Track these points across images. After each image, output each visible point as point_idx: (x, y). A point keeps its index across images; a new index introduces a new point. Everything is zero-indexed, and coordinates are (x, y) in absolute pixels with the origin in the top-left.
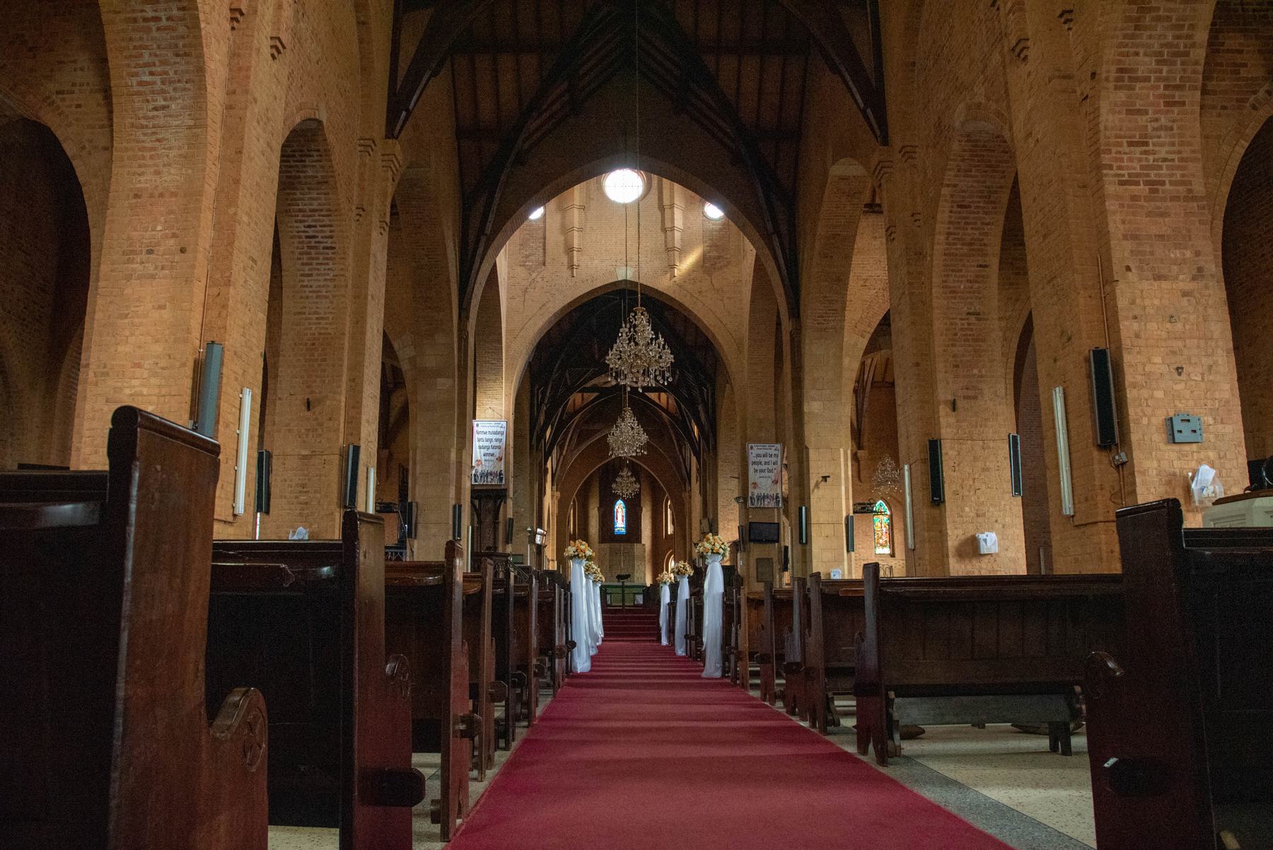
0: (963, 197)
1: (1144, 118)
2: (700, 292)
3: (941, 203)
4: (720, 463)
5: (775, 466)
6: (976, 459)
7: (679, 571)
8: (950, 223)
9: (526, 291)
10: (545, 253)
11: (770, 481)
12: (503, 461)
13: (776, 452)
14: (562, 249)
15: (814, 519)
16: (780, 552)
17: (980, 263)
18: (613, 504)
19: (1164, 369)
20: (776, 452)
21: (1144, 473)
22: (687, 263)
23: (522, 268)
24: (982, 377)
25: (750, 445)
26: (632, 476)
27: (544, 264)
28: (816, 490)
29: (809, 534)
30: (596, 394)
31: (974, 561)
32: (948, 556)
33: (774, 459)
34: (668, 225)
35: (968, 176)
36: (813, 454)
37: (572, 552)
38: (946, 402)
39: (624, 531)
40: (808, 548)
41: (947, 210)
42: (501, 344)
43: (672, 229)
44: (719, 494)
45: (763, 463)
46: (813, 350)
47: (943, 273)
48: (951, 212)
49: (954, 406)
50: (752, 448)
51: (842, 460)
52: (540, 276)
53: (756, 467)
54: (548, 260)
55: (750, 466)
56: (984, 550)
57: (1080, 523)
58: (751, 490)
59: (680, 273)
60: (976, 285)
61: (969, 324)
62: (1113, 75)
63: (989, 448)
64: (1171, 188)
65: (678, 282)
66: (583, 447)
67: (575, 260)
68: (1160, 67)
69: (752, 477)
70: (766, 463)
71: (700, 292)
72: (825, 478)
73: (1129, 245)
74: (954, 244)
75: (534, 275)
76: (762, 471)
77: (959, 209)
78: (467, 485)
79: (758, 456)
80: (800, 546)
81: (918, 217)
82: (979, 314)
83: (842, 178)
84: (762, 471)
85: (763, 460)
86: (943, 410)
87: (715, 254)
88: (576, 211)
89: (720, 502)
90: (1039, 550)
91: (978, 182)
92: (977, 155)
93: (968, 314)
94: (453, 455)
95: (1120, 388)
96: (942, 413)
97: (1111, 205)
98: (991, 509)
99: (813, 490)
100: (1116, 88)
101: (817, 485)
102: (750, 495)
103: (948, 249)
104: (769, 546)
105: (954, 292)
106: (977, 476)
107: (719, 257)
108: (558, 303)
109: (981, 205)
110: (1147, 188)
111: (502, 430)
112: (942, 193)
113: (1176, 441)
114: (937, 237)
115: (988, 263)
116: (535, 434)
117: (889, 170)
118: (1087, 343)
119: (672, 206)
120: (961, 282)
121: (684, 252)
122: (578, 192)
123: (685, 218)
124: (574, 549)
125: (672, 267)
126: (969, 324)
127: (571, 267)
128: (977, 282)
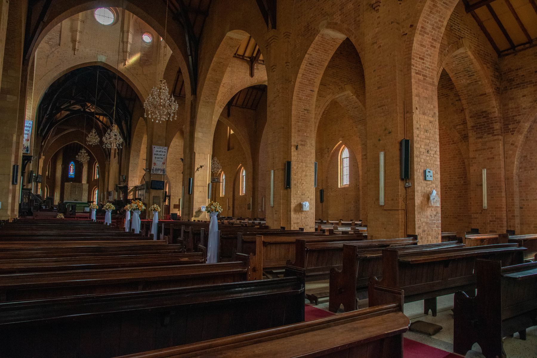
0: (312, 60)
1: (425, 49)
2: (137, 74)
3: (303, 61)
4: (132, 152)
5: (164, 157)
6: (303, 171)
7: (155, 209)
8: (305, 70)
9: (48, 56)
10: (60, 39)
11: (161, 163)
12: (29, 141)
13: (165, 151)
14: (70, 39)
15: (195, 184)
16: (163, 194)
17: (311, 89)
18: (69, 163)
19: (424, 150)
20: (165, 151)
21: (418, 191)
22: (132, 60)
23: (47, 44)
24: (307, 137)
25: (154, 146)
26: (86, 153)
27: (59, 45)
28: (197, 171)
29: (193, 190)
30: (68, 113)
31: (300, 213)
32: (290, 211)
33: (164, 153)
34: (125, 40)
35: (316, 52)
36: (197, 156)
37: (135, 207)
38: (294, 145)
39: (73, 176)
40: (192, 196)
41: (305, 64)
42: (33, 81)
43: (127, 42)
44: (130, 165)
45: (159, 155)
46: (202, 110)
47: (298, 91)
48: (306, 65)
49: (297, 147)
50: (155, 147)
51: (209, 159)
52: (57, 50)
53: (156, 156)
54: (61, 44)
55: (153, 155)
56: (304, 209)
57: (386, 209)
58: (153, 166)
59: (128, 64)
60: (309, 98)
61: (304, 114)
62: (420, 29)
63: (308, 166)
64: (429, 79)
65: (127, 68)
66: (59, 136)
67: (77, 47)
68: (432, 30)
69: (154, 160)
70: (160, 155)
71: (137, 74)
72: (201, 167)
73: (417, 98)
74: (304, 79)
75: (53, 49)
76: (158, 158)
77: (309, 65)
78: (21, 155)
79: (157, 151)
80: (188, 195)
81: (288, 64)
82: (308, 110)
83: (231, 39)
84: (158, 158)
85: (159, 153)
86: (293, 149)
87: (145, 58)
88: (79, 23)
89: (130, 169)
90: (262, 198)
91: (319, 55)
92: (322, 44)
93: (304, 110)
94: (15, 138)
95: (412, 157)
96: (292, 150)
97: (413, 81)
98: (307, 192)
99: (196, 171)
100: (420, 34)
101: (198, 169)
102: (152, 168)
103: (301, 81)
104: (159, 191)
105: (300, 99)
106: (303, 178)
107: (147, 60)
108: (65, 67)
109: (317, 65)
110: (423, 77)
111: (30, 125)
112: (306, 56)
113: (427, 180)
114: (298, 75)
115: (314, 90)
116: (40, 129)
117: (275, 40)
118: (400, 137)
119: (128, 32)
120: (304, 96)
121: (132, 54)
122: (81, 15)
123: (133, 39)
124: (136, 205)
125: (125, 60)
126: (304, 114)
127: (74, 49)
128: (309, 97)
